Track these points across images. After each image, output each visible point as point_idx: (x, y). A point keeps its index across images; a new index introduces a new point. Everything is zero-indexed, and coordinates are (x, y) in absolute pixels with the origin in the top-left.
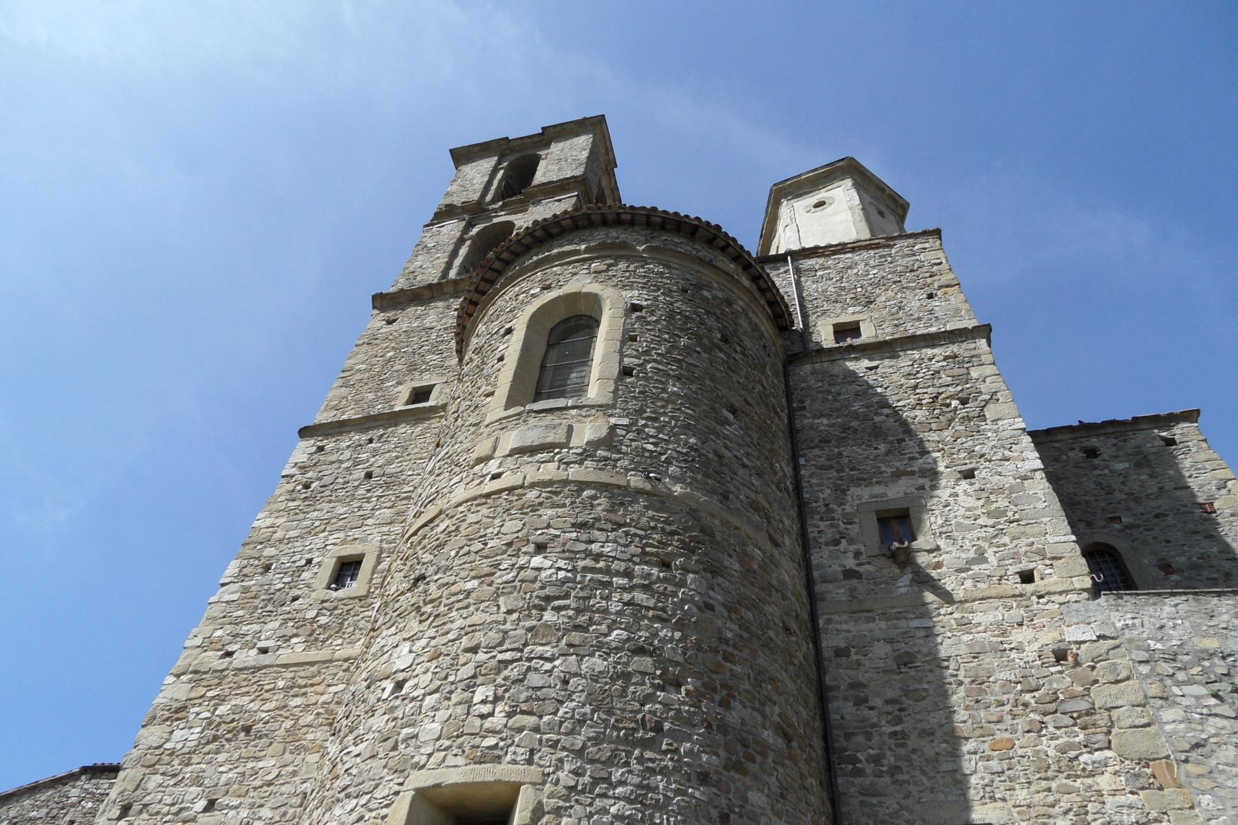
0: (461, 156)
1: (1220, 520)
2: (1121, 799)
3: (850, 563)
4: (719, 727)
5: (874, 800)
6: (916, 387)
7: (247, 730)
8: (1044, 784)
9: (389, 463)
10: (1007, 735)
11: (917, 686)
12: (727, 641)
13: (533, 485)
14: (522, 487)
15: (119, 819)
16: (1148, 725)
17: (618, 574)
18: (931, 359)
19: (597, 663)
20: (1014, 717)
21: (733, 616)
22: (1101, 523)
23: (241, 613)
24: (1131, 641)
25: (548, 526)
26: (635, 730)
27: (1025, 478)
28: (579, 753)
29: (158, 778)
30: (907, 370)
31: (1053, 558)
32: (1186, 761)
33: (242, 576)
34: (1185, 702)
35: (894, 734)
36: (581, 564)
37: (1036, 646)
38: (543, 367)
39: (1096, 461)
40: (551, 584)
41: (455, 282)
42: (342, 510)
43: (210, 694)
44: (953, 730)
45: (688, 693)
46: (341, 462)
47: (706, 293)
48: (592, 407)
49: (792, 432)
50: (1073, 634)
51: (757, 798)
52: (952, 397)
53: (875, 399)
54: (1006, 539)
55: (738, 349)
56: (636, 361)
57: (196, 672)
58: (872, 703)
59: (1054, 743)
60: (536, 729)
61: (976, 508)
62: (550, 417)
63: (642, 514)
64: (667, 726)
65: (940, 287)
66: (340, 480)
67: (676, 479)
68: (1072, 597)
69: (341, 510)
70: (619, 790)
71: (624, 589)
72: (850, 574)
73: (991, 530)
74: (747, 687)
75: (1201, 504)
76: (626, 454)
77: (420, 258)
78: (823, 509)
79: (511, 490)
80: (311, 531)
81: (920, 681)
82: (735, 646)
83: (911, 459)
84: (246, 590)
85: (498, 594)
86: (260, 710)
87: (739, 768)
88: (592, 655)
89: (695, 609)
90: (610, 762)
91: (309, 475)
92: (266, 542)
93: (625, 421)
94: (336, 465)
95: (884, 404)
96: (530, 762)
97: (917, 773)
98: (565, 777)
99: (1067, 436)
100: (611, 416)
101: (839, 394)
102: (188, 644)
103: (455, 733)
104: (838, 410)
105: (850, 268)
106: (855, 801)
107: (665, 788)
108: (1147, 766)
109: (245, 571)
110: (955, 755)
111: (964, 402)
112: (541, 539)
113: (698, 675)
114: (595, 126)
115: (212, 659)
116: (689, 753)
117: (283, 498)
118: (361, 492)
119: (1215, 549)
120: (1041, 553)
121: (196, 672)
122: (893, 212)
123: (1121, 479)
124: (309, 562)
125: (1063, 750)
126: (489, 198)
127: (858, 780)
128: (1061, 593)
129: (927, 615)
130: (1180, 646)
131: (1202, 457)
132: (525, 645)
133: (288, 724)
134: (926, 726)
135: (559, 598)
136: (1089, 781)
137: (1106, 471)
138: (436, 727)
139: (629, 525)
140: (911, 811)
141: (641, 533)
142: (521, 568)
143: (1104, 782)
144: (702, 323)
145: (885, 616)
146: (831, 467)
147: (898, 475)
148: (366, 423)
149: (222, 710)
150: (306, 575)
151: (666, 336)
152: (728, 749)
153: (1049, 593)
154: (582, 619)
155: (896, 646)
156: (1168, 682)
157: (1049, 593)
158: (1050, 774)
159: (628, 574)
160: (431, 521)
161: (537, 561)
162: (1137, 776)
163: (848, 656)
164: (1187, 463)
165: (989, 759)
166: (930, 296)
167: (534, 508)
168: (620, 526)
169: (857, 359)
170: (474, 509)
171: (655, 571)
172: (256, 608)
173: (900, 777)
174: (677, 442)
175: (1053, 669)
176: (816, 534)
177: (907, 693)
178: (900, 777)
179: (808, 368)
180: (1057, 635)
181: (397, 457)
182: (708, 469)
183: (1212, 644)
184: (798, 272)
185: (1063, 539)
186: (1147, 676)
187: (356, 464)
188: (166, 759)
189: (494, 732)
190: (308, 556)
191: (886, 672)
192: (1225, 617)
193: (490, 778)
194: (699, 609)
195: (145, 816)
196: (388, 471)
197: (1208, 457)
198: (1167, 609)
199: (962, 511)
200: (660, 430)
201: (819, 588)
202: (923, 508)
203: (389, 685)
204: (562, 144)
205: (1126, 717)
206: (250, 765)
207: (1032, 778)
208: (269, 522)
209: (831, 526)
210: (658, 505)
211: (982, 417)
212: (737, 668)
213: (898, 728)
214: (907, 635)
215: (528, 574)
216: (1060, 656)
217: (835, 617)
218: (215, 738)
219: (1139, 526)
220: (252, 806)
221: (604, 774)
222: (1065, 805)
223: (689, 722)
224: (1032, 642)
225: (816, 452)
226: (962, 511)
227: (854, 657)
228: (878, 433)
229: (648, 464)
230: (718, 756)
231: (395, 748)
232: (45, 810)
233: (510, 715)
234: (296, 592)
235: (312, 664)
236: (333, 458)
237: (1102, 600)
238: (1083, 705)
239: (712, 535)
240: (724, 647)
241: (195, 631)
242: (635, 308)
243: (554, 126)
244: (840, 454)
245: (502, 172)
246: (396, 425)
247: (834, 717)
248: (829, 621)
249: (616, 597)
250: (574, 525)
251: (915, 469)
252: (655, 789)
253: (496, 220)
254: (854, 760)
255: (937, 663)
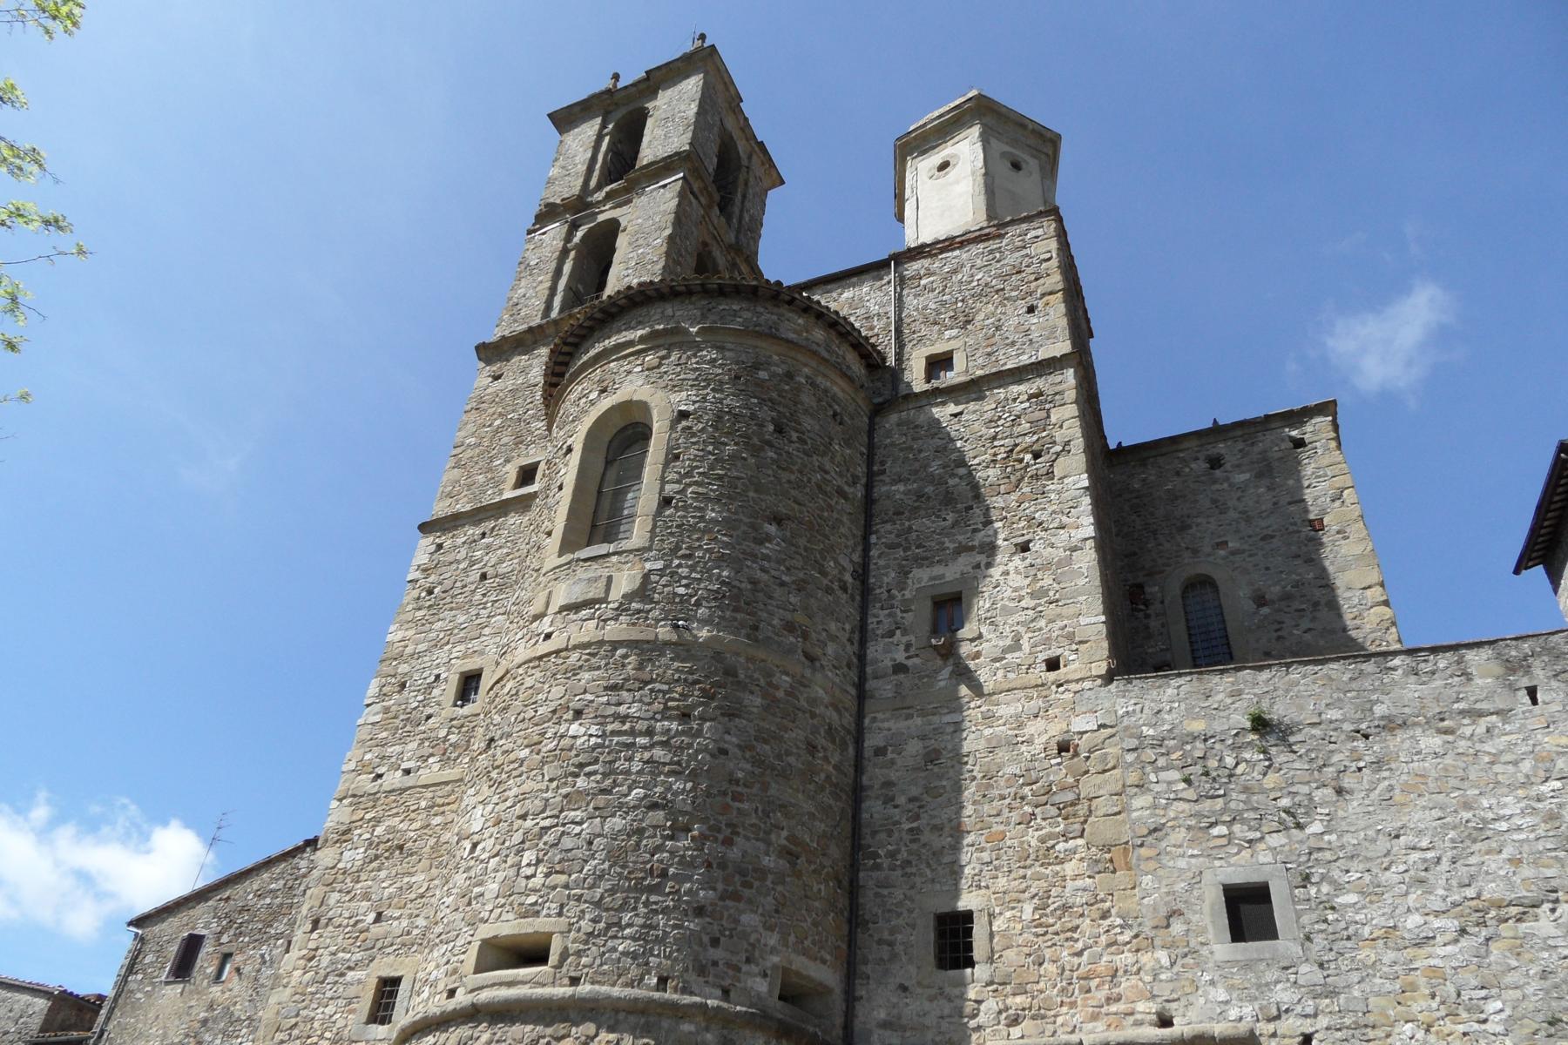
0: (564, 119)
1: (1325, 539)
2: (1079, 883)
3: (900, 656)
4: (719, 865)
5: (885, 892)
6: (994, 438)
7: (401, 848)
8: (1021, 872)
9: (501, 561)
10: (1002, 828)
11: (937, 783)
12: (737, 782)
13: (575, 647)
14: (566, 649)
15: (312, 931)
16: (1119, 813)
17: (641, 734)
18: (1015, 400)
19: (617, 822)
20: (1011, 809)
21: (748, 754)
22: (1207, 549)
23: (384, 734)
24: (1127, 728)
25: (585, 692)
26: (644, 879)
27: (1074, 549)
28: (598, 904)
29: (335, 896)
30: (989, 415)
31: (1081, 642)
32: (1142, 845)
33: (382, 696)
34: (1158, 788)
35: (911, 830)
36: (610, 728)
37: (1044, 738)
38: (599, 492)
39: (1218, 473)
40: (585, 751)
41: (555, 322)
42: (461, 619)
43: (368, 816)
44: (959, 824)
45: (693, 838)
46: (458, 562)
47: (763, 375)
48: (630, 551)
49: (869, 501)
50: (1081, 723)
51: (749, 919)
52: (1025, 450)
53: (953, 457)
54: (1042, 623)
55: (795, 436)
56: (677, 487)
57: (354, 796)
58: (898, 801)
59: (1037, 834)
60: (566, 886)
61: (1022, 588)
62: (595, 566)
63: (668, 667)
64: (671, 871)
65: (1043, 295)
66: (459, 584)
67: (704, 622)
68: (1087, 685)
69: (461, 619)
70: (627, 931)
71: (645, 748)
72: (899, 668)
73: (1030, 612)
74: (754, 821)
75: (1311, 521)
76: (657, 603)
77: (523, 283)
78: (885, 595)
79: (557, 652)
80: (437, 645)
81: (940, 777)
82: (745, 785)
83: (975, 531)
84: (386, 710)
85: (543, 763)
86: (409, 829)
87: (736, 897)
88: (613, 815)
89: (708, 757)
90: (622, 908)
91: (431, 579)
92: (399, 657)
93: (659, 565)
94: (454, 566)
95: (962, 463)
96: (560, 914)
97: (923, 866)
98: (585, 925)
99: (1193, 443)
100: (647, 560)
101: (920, 451)
102: (345, 768)
103: (508, 891)
104: (916, 472)
105: (955, 272)
106: (870, 894)
107: (665, 925)
108: (1109, 851)
109: (385, 690)
110: (956, 848)
111: (1037, 456)
112: (578, 706)
113: (703, 821)
114: (703, 59)
115: (365, 782)
116: (689, 892)
117: (410, 607)
118: (478, 597)
119: (1311, 575)
120: (1070, 637)
121: (354, 796)
122: (1036, 152)
123: (1239, 494)
124: (438, 677)
125: (1042, 840)
126: (593, 183)
127: (875, 874)
128: (1077, 681)
129: (959, 709)
130: (1170, 731)
131: (1326, 461)
132: (561, 811)
133: (432, 841)
134: (937, 821)
135: (590, 764)
136: (1058, 868)
137: (1225, 485)
138: (495, 886)
139: (652, 681)
140: (912, 901)
141: (665, 687)
142: (562, 736)
143: (1070, 868)
144: (753, 417)
145: (923, 713)
146: (899, 545)
147: (963, 549)
148: (477, 515)
149: (379, 830)
150: (436, 692)
151: (710, 448)
152: (726, 881)
153: (1067, 682)
154: (608, 782)
155: (928, 743)
156: (1149, 769)
157: (1067, 682)
158: (1029, 862)
159: (650, 732)
160: (501, 679)
161: (575, 728)
162: (1097, 861)
163: (885, 754)
164: (1309, 470)
165: (982, 850)
166: (1031, 310)
167: (576, 671)
168: (647, 683)
169: (943, 403)
170: (530, 672)
171: (674, 726)
172: (397, 728)
173: (909, 870)
174: (709, 579)
175: (1053, 762)
176: (874, 626)
177: (927, 790)
178: (909, 870)
179: (894, 418)
180: (1064, 726)
181: (508, 554)
182: (738, 604)
183: (1198, 726)
184: (902, 281)
185: (1093, 620)
186: (1131, 764)
187: (472, 564)
188: (340, 877)
189: (535, 891)
190: (436, 672)
191: (915, 769)
192: (1221, 696)
193: (530, 930)
194: (713, 756)
195: (330, 928)
196: (501, 571)
197: (1332, 460)
198: (1170, 691)
199: (1009, 593)
200: (692, 568)
201: (871, 684)
202: (976, 592)
203: (467, 845)
204: (669, 92)
205: (1103, 806)
206: (406, 880)
207: (1014, 866)
208: (400, 635)
209: (889, 615)
210: (684, 654)
211: (1050, 474)
212: (745, 806)
213: (914, 825)
214: (938, 731)
215: (566, 742)
216: (1063, 748)
217: (880, 716)
218: (377, 857)
219: (1243, 551)
220: (410, 916)
221: (615, 920)
222: (1033, 890)
223: (691, 865)
224: (1043, 733)
225: (888, 526)
226: (1009, 593)
227: (890, 756)
228: (949, 500)
229: (679, 611)
230: (714, 889)
231: (469, 904)
232: (282, 882)
233: (547, 875)
234: (429, 711)
235: (446, 783)
236: (450, 558)
237: (1112, 687)
238: (1070, 796)
239: (735, 675)
240: (735, 788)
241: (349, 755)
242: (684, 415)
243: (659, 68)
244: (910, 528)
245: (607, 139)
246: (506, 515)
247: (865, 816)
248: (874, 720)
249: (638, 756)
250: (606, 688)
251: (976, 543)
252: (655, 927)
253: (601, 218)
254: (875, 855)
255: (958, 759)
